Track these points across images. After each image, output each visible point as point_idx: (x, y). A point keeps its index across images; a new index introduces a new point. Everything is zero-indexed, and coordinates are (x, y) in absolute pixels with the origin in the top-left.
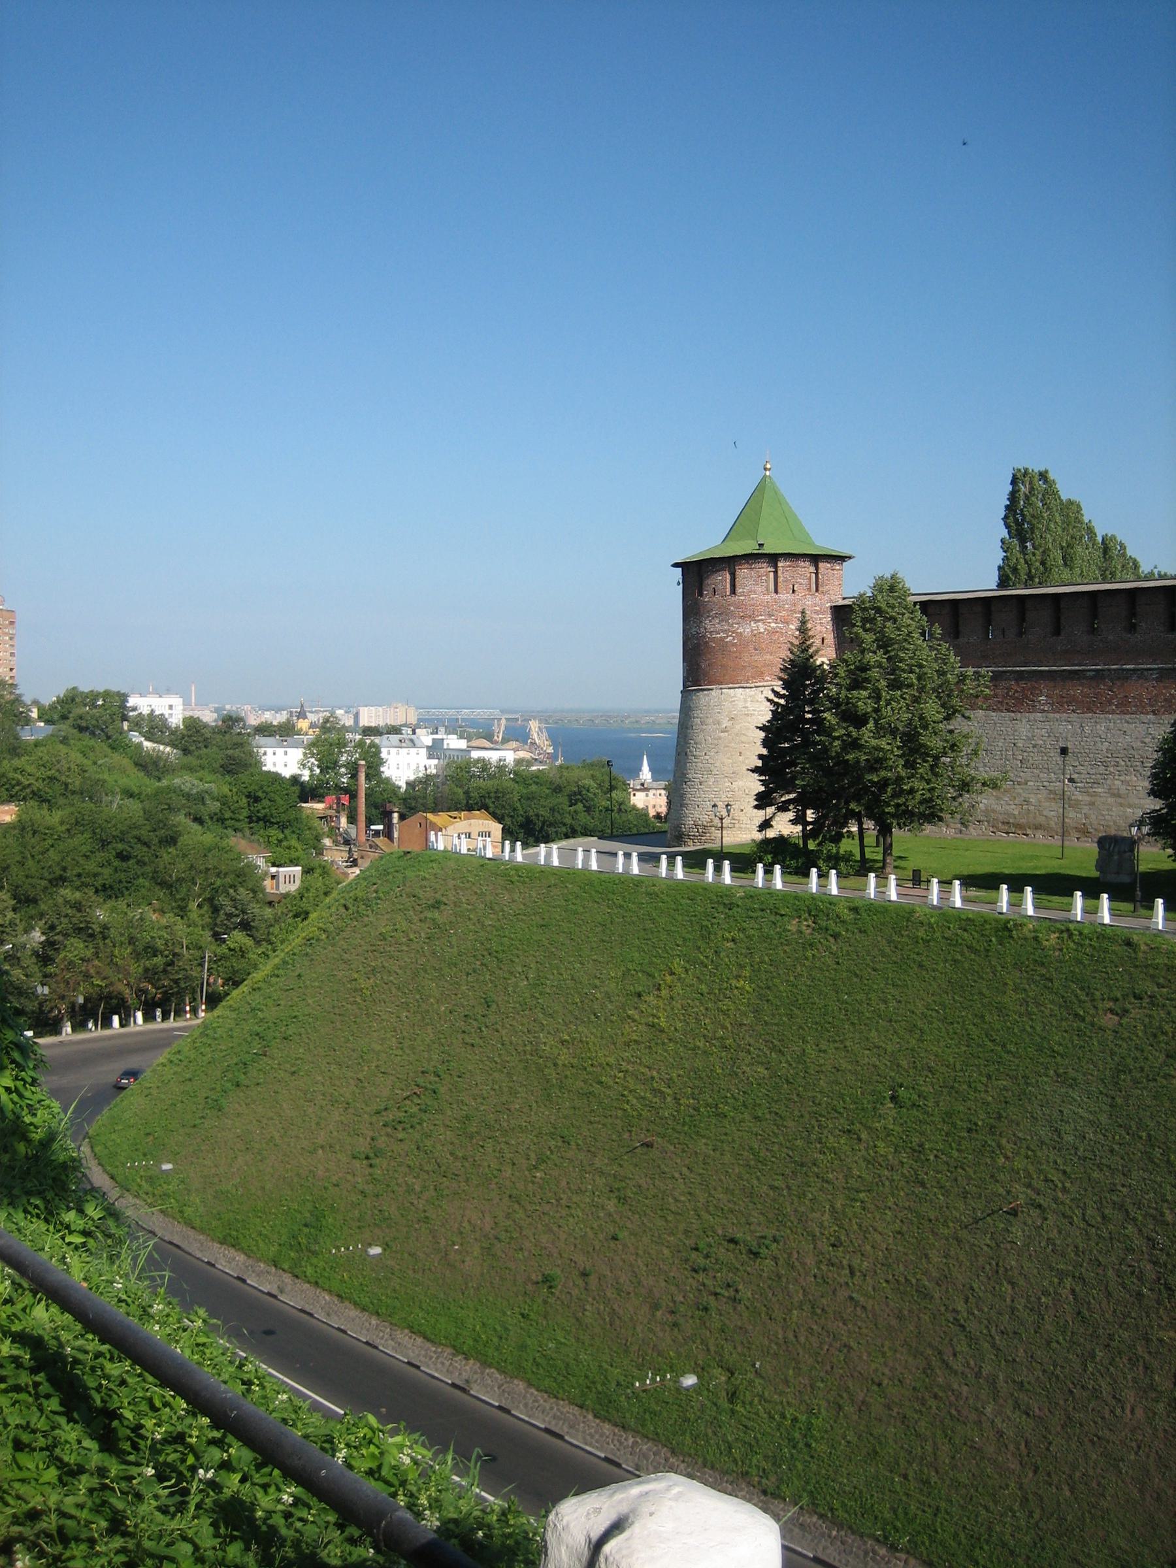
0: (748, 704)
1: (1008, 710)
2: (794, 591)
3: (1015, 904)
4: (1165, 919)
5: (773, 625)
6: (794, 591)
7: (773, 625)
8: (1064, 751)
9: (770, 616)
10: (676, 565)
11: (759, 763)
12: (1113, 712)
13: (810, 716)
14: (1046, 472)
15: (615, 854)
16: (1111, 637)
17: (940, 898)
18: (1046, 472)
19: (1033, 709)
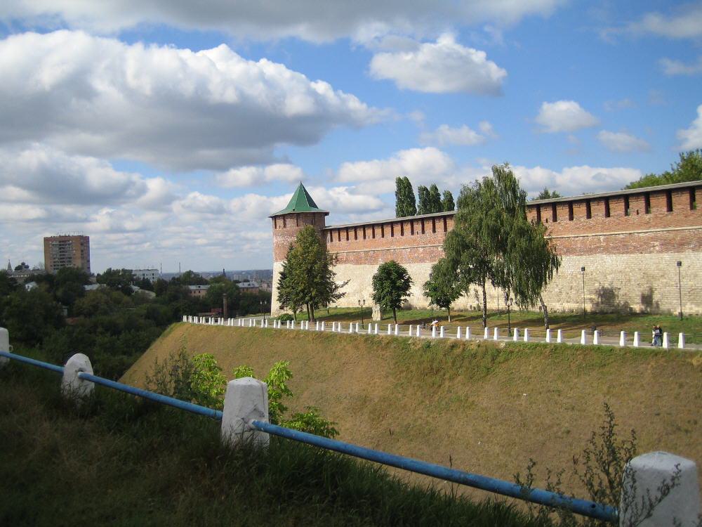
4: (625, 340)
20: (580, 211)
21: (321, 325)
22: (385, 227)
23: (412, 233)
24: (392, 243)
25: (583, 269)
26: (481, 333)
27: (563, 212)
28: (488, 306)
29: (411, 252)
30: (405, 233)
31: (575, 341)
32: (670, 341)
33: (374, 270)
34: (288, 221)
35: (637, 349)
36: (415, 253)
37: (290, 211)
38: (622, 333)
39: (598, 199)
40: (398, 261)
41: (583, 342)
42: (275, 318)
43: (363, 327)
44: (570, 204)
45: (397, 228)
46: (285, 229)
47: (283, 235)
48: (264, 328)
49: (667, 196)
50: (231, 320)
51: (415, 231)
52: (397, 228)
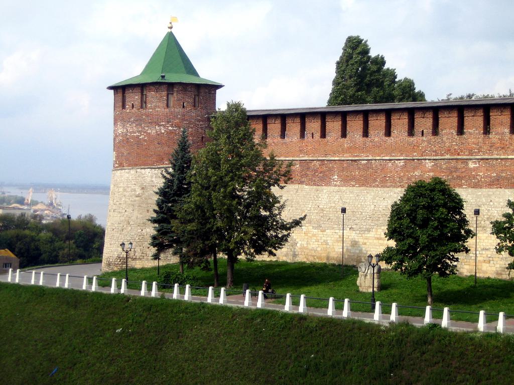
0: (154, 179)
1: (315, 185)
2: (183, 107)
3: (14, 277)
4: (505, 324)
5: (170, 128)
6: (183, 107)
7: (170, 128)
8: (344, 210)
9: (168, 122)
10: (111, 88)
11: (155, 215)
12: (378, 186)
13: (186, 186)
14: (172, 49)
15: (40, 273)
16: (376, 139)
17: (11, 279)
18: (172, 49)
19: (328, 184)
20: (449, 122)
21: (15, 276)
22: (328, 119)
23: (411, 132)
24: (363, 149)
25: (344, 210)
26: (281, 299)
27: (424, 123)
28: (477, 275)
29: (405, 166)
30: (395, 132)
31: (203, 299)
32: (35, 278)
33: (394, 195)
34: (151, 95)
35: (261, 310)
36: (415, 169)
37: (156, 78)
38: (501, 314)
39: (474, 107)
40: (451, 184)
41: (9, 280)
42: (114, 274)
43: (318, 303)
44: (436, 111)
45: (334, 126)
46: (143, 111)
47: (139, 121)
48: (179, 303)
49: (281, 121)
50: (14, 271)
51: (418, 129)
52: (334, 126)
